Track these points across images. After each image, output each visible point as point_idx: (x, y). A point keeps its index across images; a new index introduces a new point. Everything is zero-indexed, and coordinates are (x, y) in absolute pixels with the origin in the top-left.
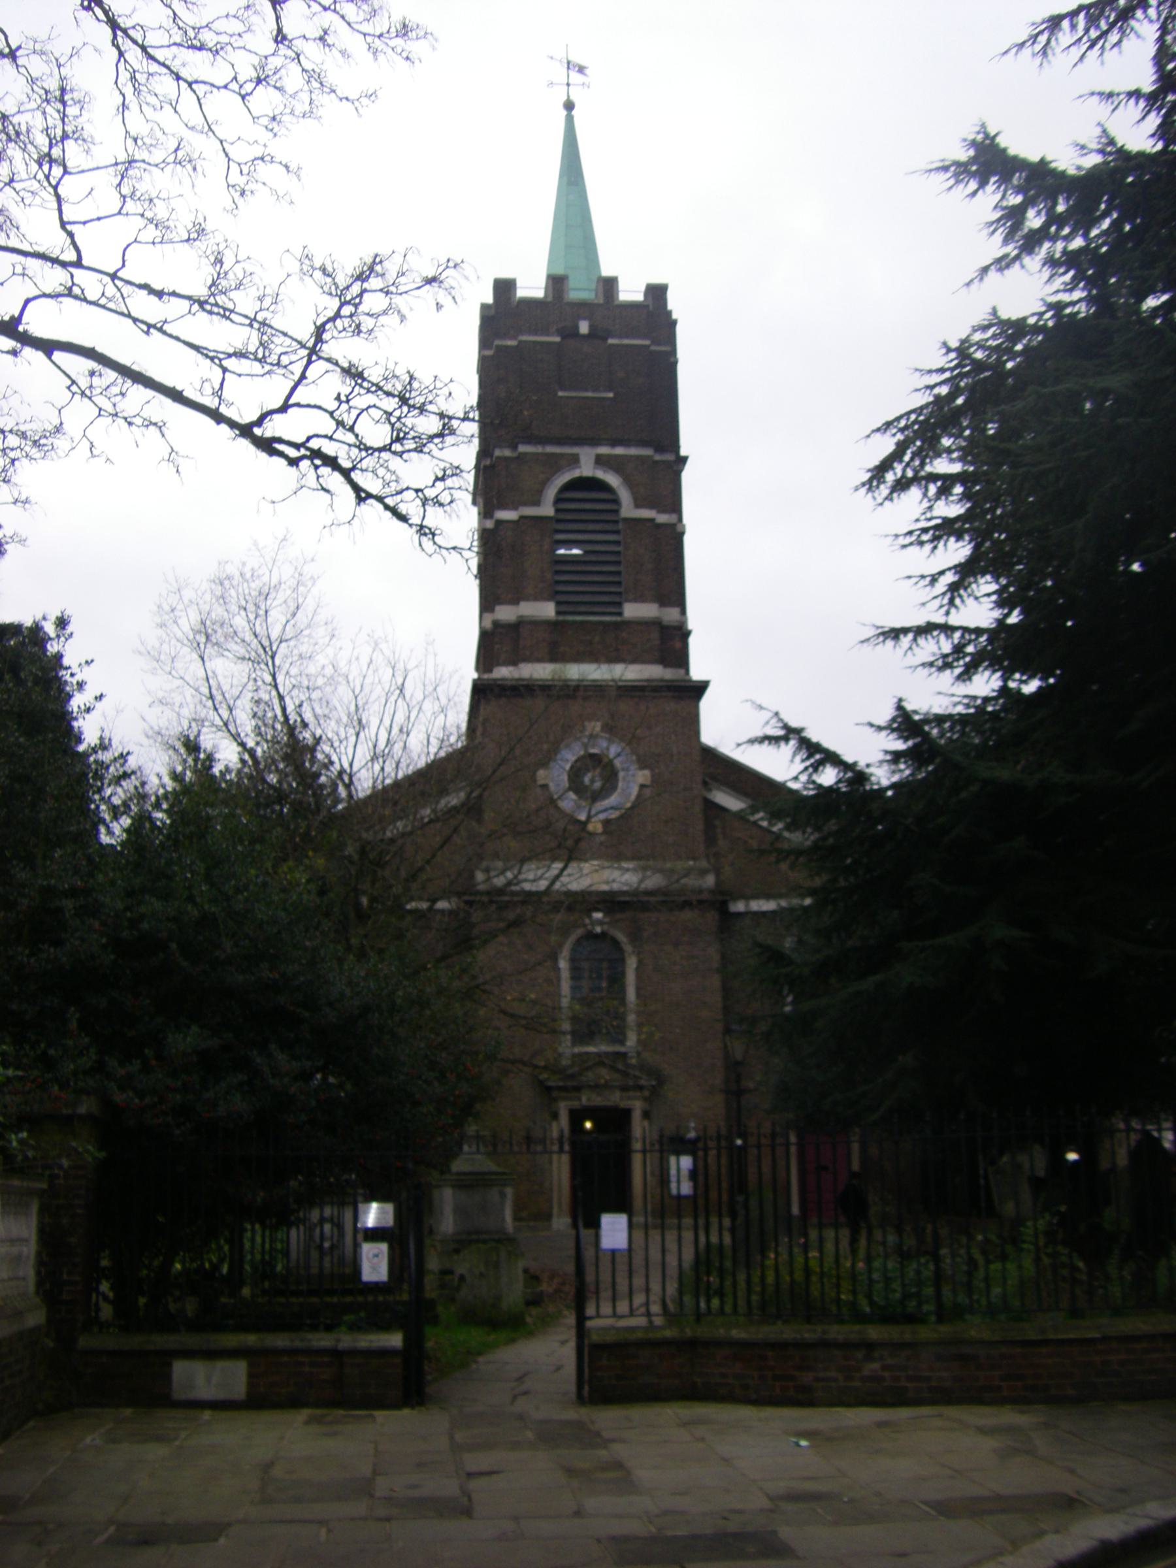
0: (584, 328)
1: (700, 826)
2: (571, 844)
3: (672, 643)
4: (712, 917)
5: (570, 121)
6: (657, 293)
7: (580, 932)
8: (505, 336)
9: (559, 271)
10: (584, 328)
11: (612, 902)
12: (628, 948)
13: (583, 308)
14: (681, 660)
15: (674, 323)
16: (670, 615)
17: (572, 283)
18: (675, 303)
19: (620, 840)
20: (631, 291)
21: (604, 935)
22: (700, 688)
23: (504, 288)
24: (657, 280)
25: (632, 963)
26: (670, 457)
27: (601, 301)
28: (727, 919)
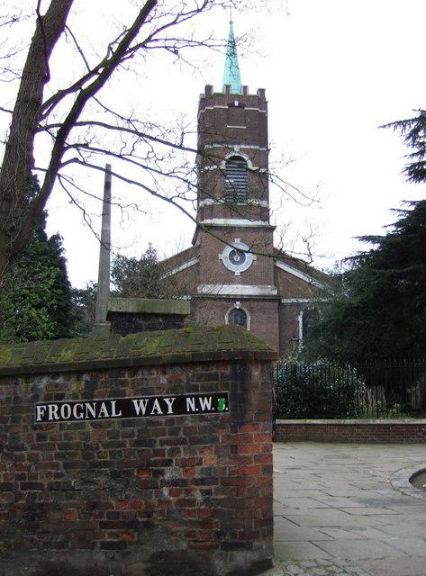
0: (236, 103)
1: (272, 274)
2: (229, 278)
3: (264, 213)
4: (276, 304)
5: (231, 27)
6: (262, 91)
7: (232, 308)
8: (209, 105)
9: (227, 83)
10: (236, 103)
11: (243, 299)
12: (248, 313)
13: (237, 96)
14: (267, 218)
15: (266, 103)
16: (264, 203)
17: (232, 87)
18: (268, 97)
19: (246, 278)
20: (252, 91)
21: (240, 309)
22: (273, 228)
23: (209, 88)
24: (108, 163)
25: (249, 319)
26: (265, 149)
27: (242, 94)
28: (280, 303)
